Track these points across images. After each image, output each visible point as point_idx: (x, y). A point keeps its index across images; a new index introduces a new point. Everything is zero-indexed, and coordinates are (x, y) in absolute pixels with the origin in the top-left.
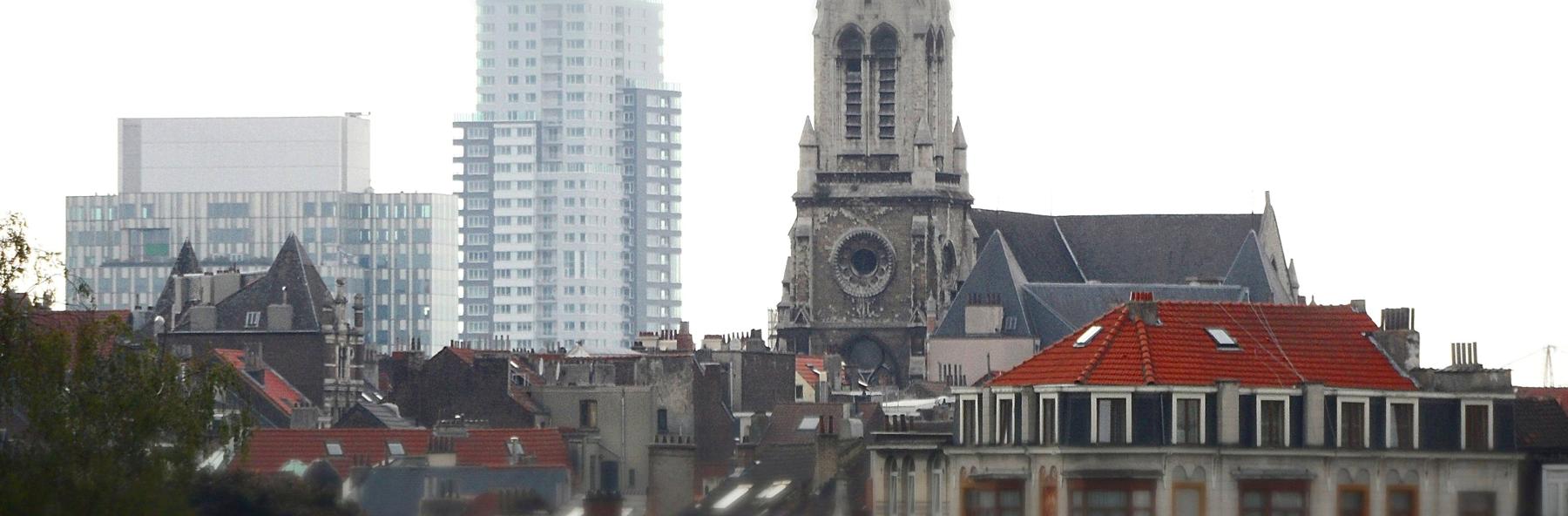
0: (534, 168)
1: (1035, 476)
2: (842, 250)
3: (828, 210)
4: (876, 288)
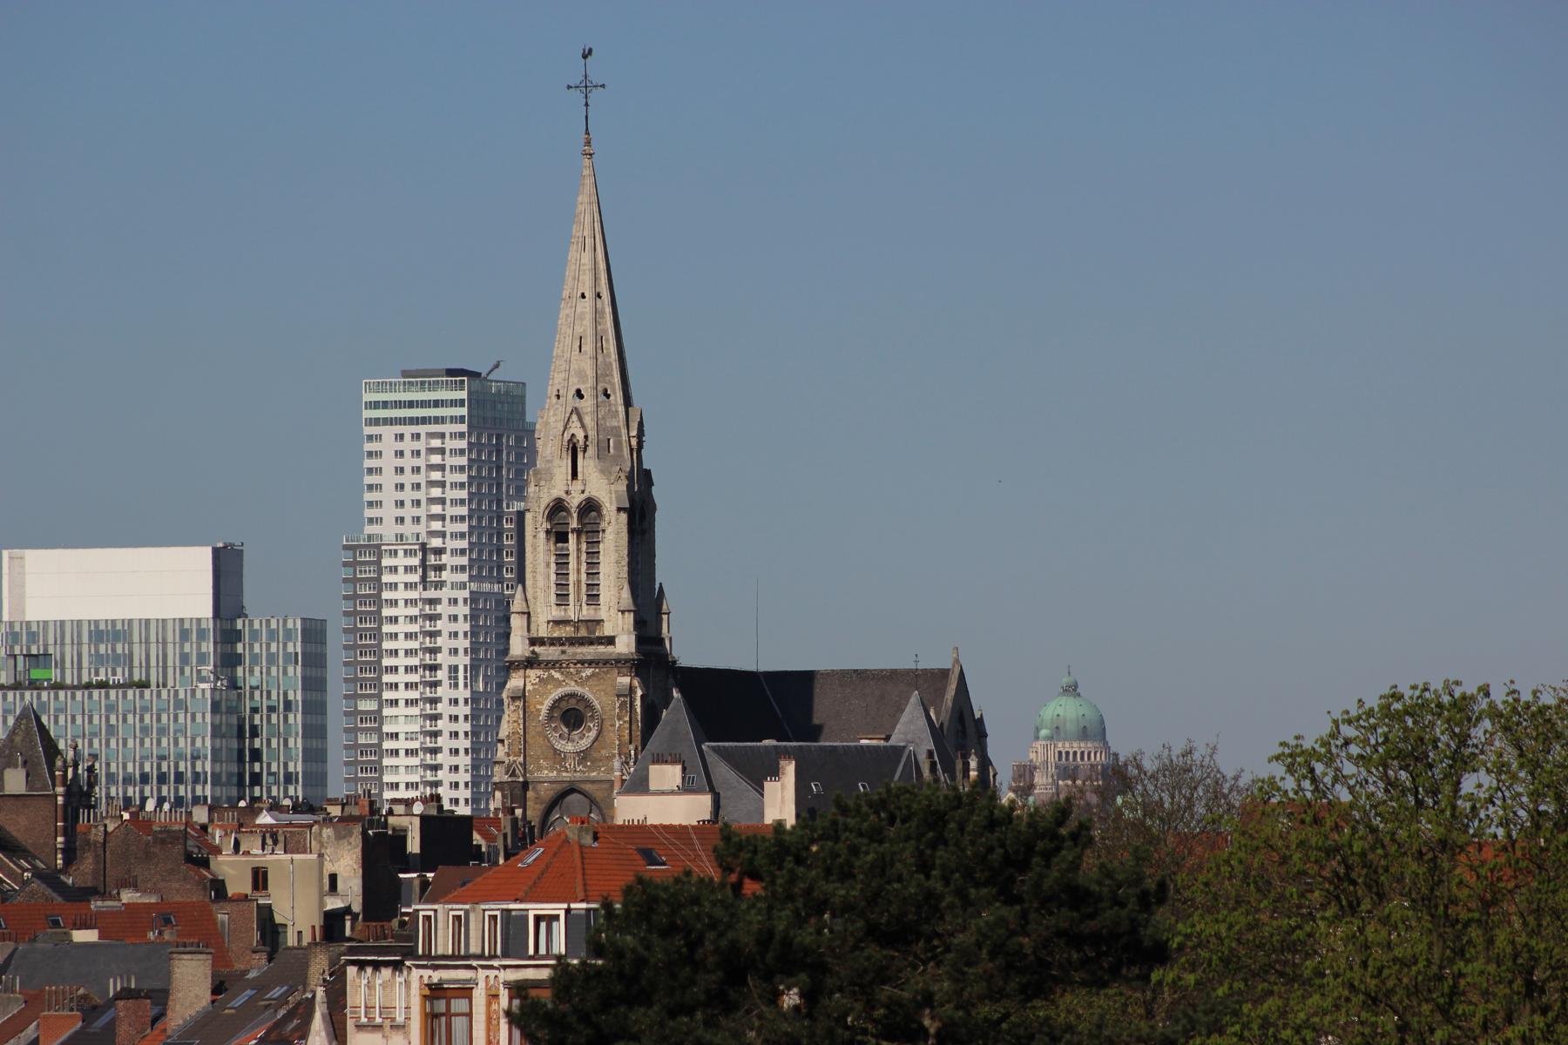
0: (420, 587)
1: (482, 984)
2: (552, 708)
3: (539, 672)
4: (584, 743)
